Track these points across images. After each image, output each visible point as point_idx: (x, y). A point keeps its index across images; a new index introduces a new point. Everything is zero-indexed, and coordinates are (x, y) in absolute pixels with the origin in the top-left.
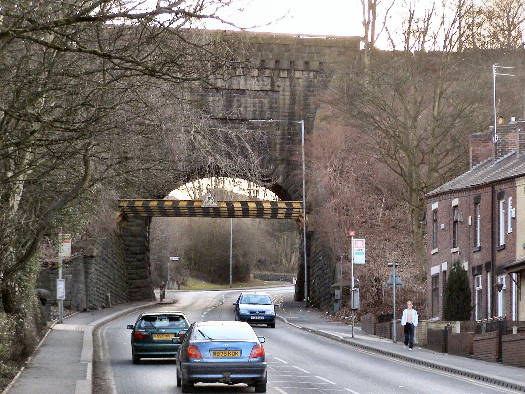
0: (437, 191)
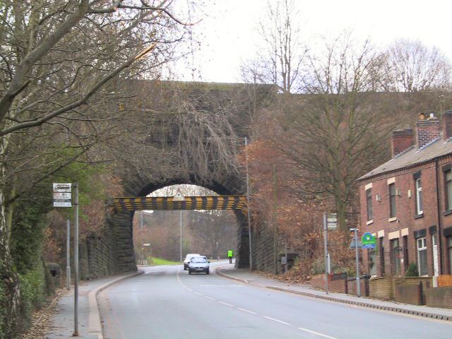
0: (369, 174)
